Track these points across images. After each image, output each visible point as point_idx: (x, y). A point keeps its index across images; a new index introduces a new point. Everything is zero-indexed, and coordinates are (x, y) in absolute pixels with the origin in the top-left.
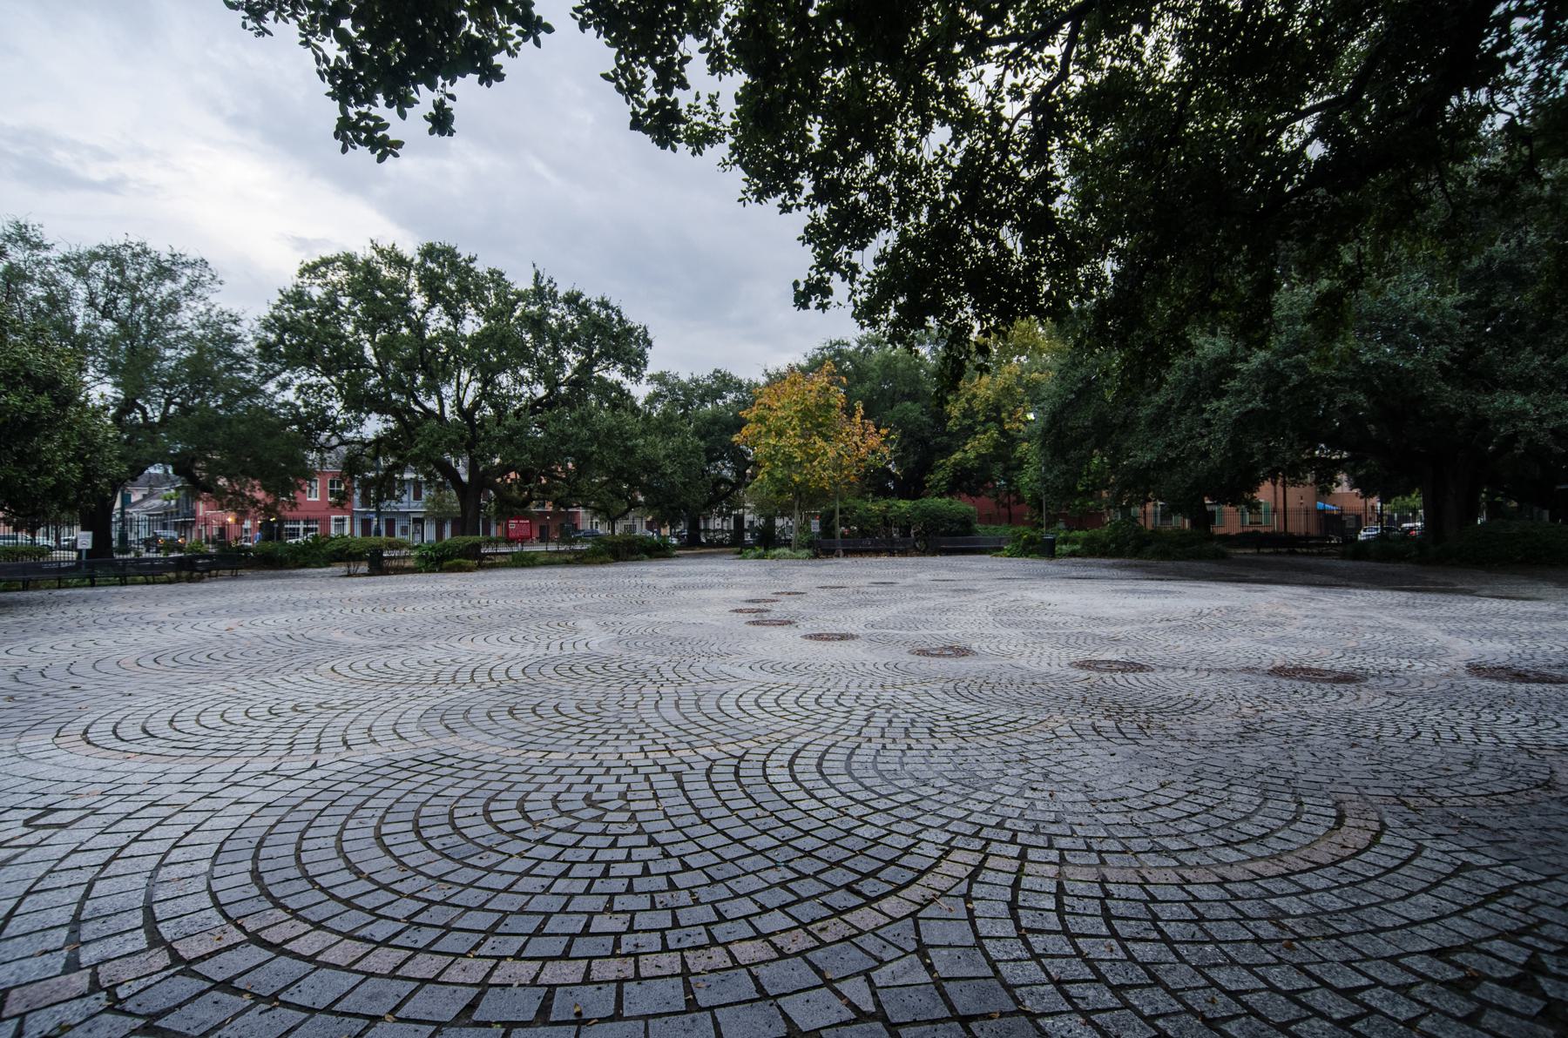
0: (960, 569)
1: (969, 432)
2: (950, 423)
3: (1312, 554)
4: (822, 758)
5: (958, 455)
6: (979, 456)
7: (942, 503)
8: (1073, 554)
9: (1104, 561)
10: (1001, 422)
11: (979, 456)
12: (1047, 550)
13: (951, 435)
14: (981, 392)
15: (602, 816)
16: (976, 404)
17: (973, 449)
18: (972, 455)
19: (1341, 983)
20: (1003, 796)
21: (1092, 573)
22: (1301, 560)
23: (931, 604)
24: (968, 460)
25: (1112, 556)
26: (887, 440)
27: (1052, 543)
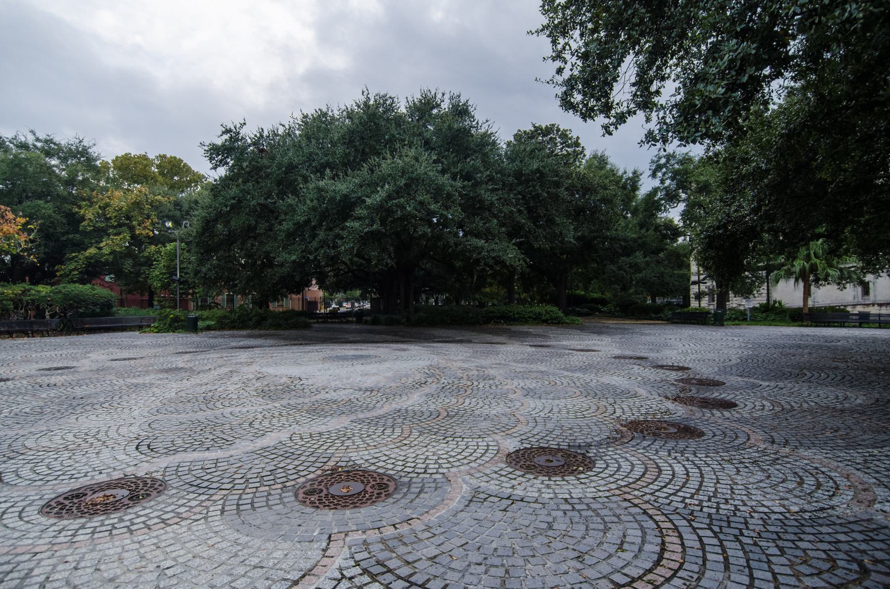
0: (129, 347)
1: (100, 233)
2: (85, 223)
3: (334, 323)
4: (658, 476)
5: (92, 251)
6: (113, 252)
7: (79, 288)
8: (208, 328)
9: (244, 332)
10: (132, 229)
11: (113, 252)
12: (192, 326)
13: (85, 233)
14: (115, 203)
15: (801, 511)
16: (110, 213)
17: (109, 245)
18: (106, 251)
19: (22, 565)
20: (96, 527)
21: (364, 353)
22: (329, 326)
23: (195, 380)
24: (103, 255)
25: (254, 327)
26: (25, 228)
27: (196, 320)
